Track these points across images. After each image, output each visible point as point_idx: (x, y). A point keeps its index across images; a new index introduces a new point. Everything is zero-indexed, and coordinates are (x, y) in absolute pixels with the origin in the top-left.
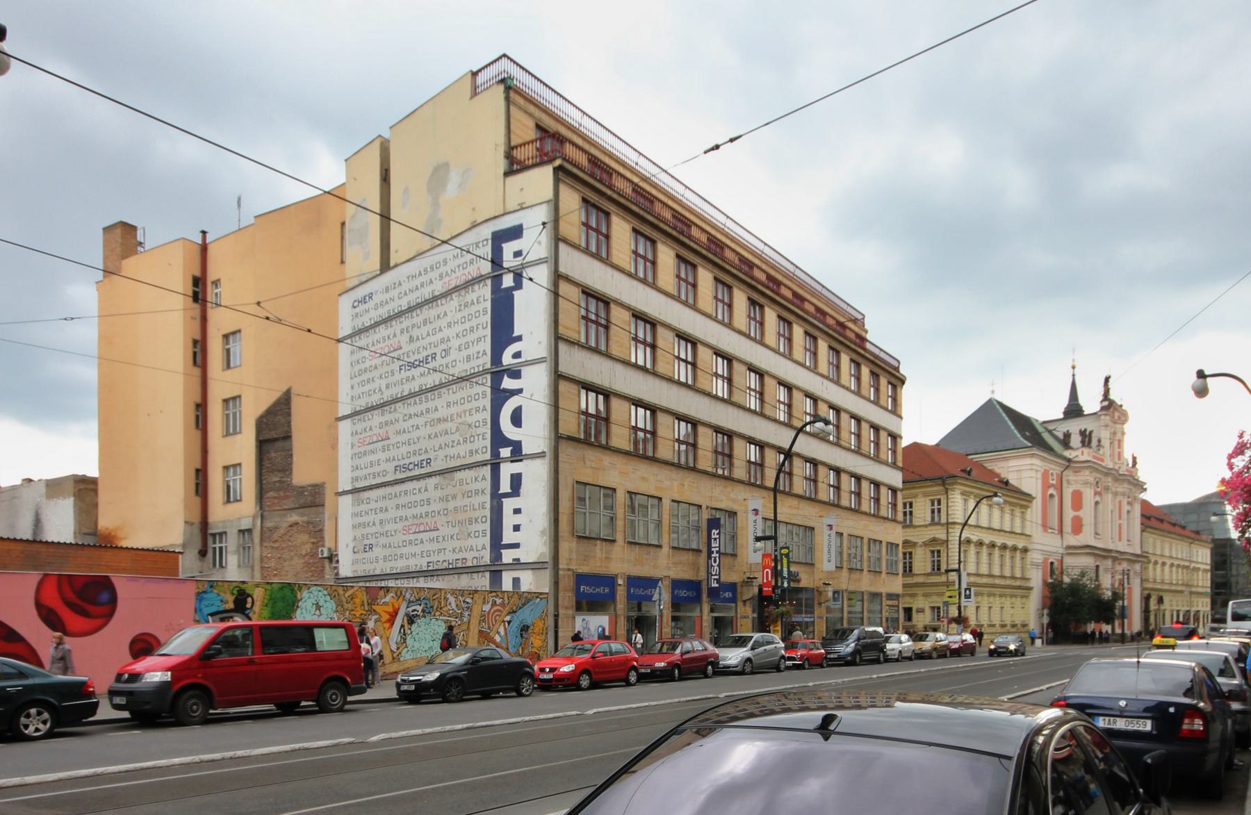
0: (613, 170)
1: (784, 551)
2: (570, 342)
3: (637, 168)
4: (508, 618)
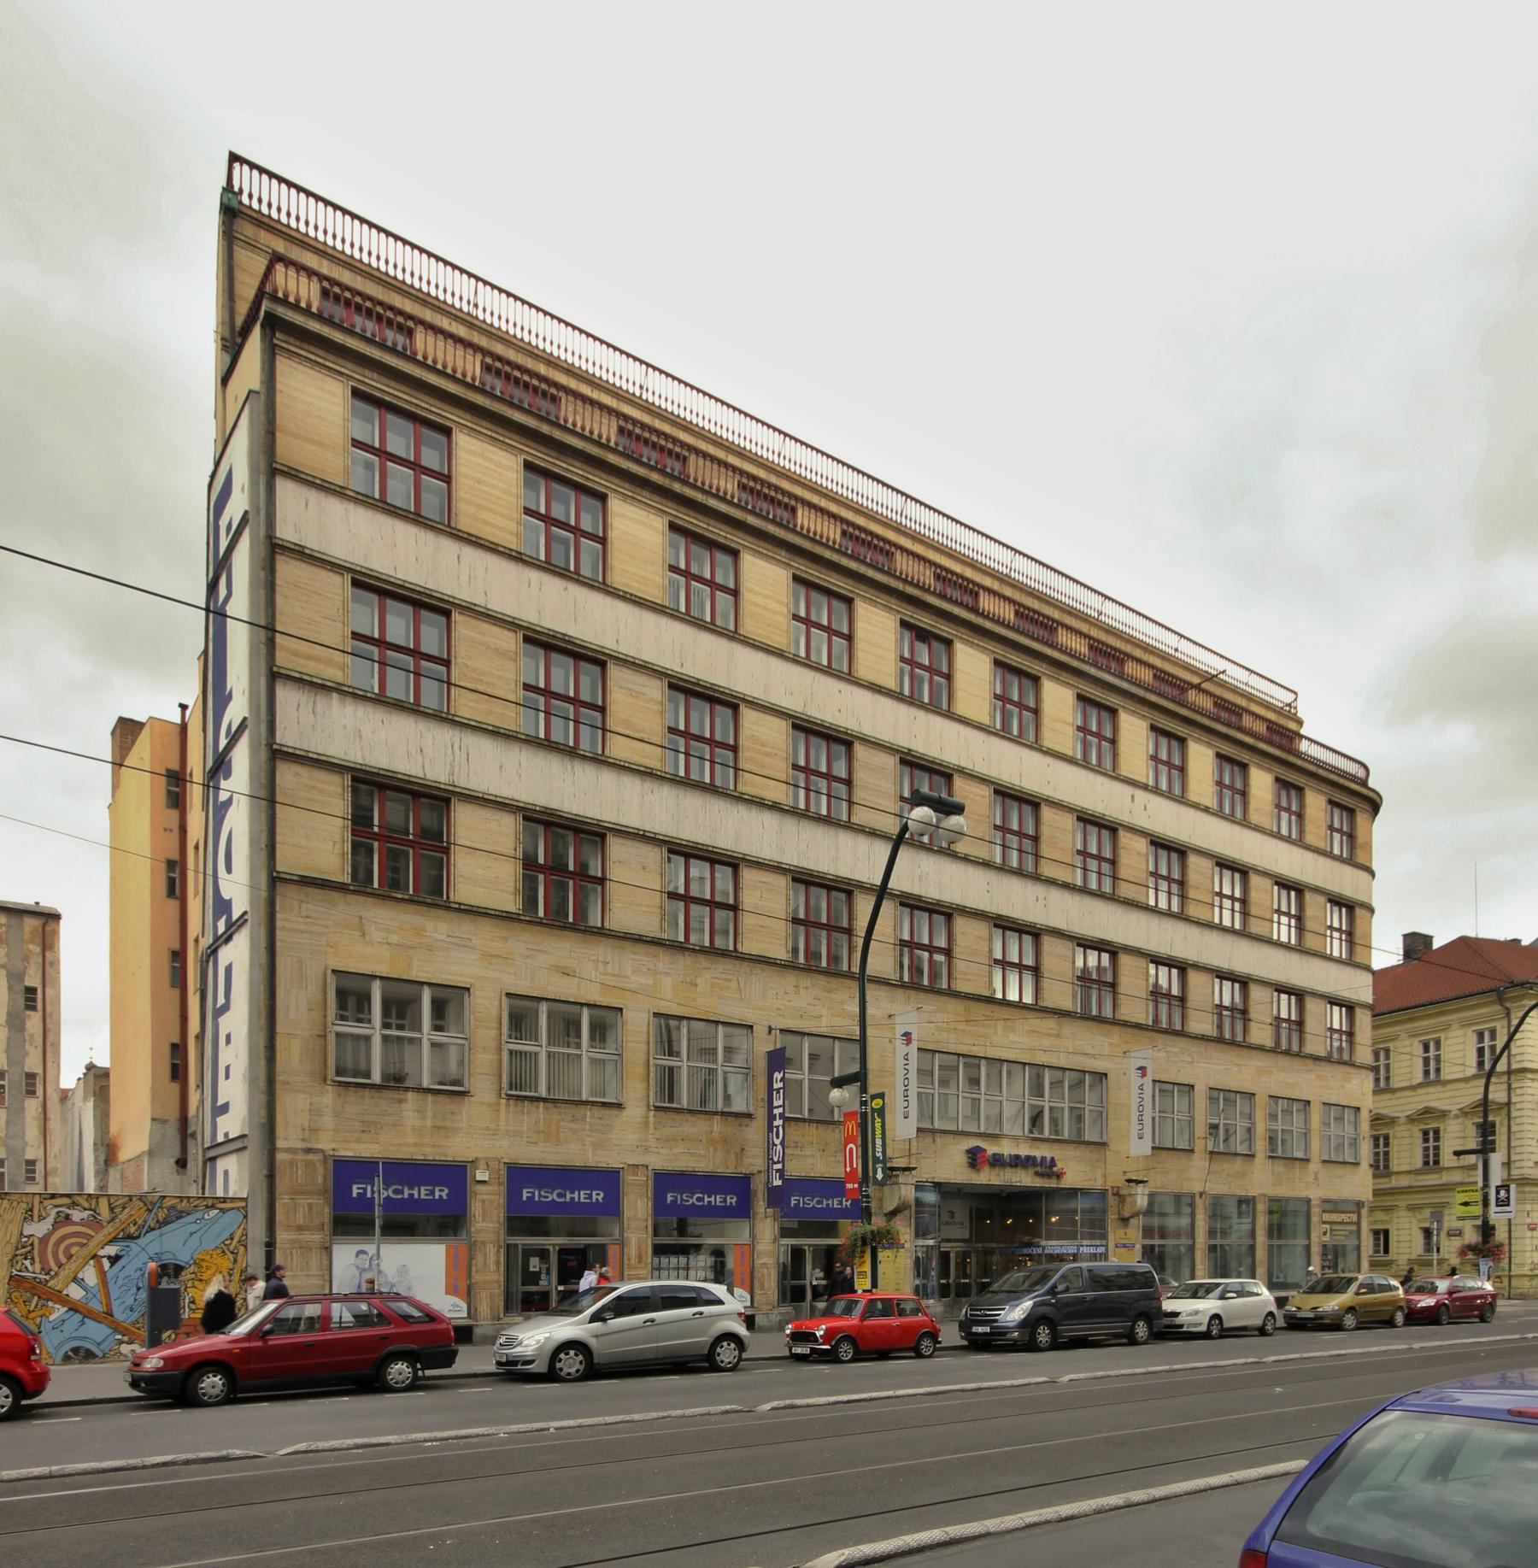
0: (978, 585)
1: (877, 1103)
2: (312, 684)
3: (1178, 655)
4: (112, 1250)
